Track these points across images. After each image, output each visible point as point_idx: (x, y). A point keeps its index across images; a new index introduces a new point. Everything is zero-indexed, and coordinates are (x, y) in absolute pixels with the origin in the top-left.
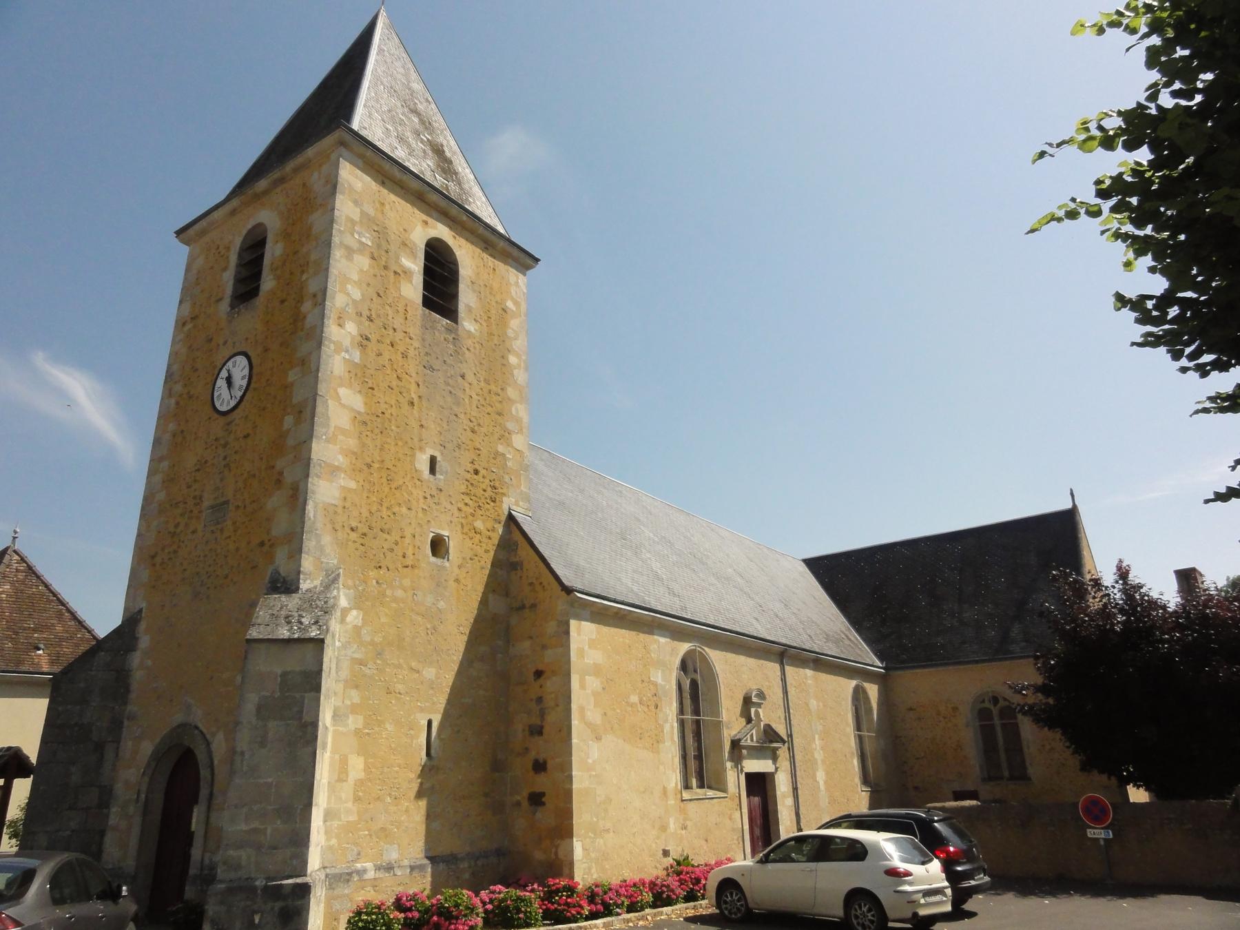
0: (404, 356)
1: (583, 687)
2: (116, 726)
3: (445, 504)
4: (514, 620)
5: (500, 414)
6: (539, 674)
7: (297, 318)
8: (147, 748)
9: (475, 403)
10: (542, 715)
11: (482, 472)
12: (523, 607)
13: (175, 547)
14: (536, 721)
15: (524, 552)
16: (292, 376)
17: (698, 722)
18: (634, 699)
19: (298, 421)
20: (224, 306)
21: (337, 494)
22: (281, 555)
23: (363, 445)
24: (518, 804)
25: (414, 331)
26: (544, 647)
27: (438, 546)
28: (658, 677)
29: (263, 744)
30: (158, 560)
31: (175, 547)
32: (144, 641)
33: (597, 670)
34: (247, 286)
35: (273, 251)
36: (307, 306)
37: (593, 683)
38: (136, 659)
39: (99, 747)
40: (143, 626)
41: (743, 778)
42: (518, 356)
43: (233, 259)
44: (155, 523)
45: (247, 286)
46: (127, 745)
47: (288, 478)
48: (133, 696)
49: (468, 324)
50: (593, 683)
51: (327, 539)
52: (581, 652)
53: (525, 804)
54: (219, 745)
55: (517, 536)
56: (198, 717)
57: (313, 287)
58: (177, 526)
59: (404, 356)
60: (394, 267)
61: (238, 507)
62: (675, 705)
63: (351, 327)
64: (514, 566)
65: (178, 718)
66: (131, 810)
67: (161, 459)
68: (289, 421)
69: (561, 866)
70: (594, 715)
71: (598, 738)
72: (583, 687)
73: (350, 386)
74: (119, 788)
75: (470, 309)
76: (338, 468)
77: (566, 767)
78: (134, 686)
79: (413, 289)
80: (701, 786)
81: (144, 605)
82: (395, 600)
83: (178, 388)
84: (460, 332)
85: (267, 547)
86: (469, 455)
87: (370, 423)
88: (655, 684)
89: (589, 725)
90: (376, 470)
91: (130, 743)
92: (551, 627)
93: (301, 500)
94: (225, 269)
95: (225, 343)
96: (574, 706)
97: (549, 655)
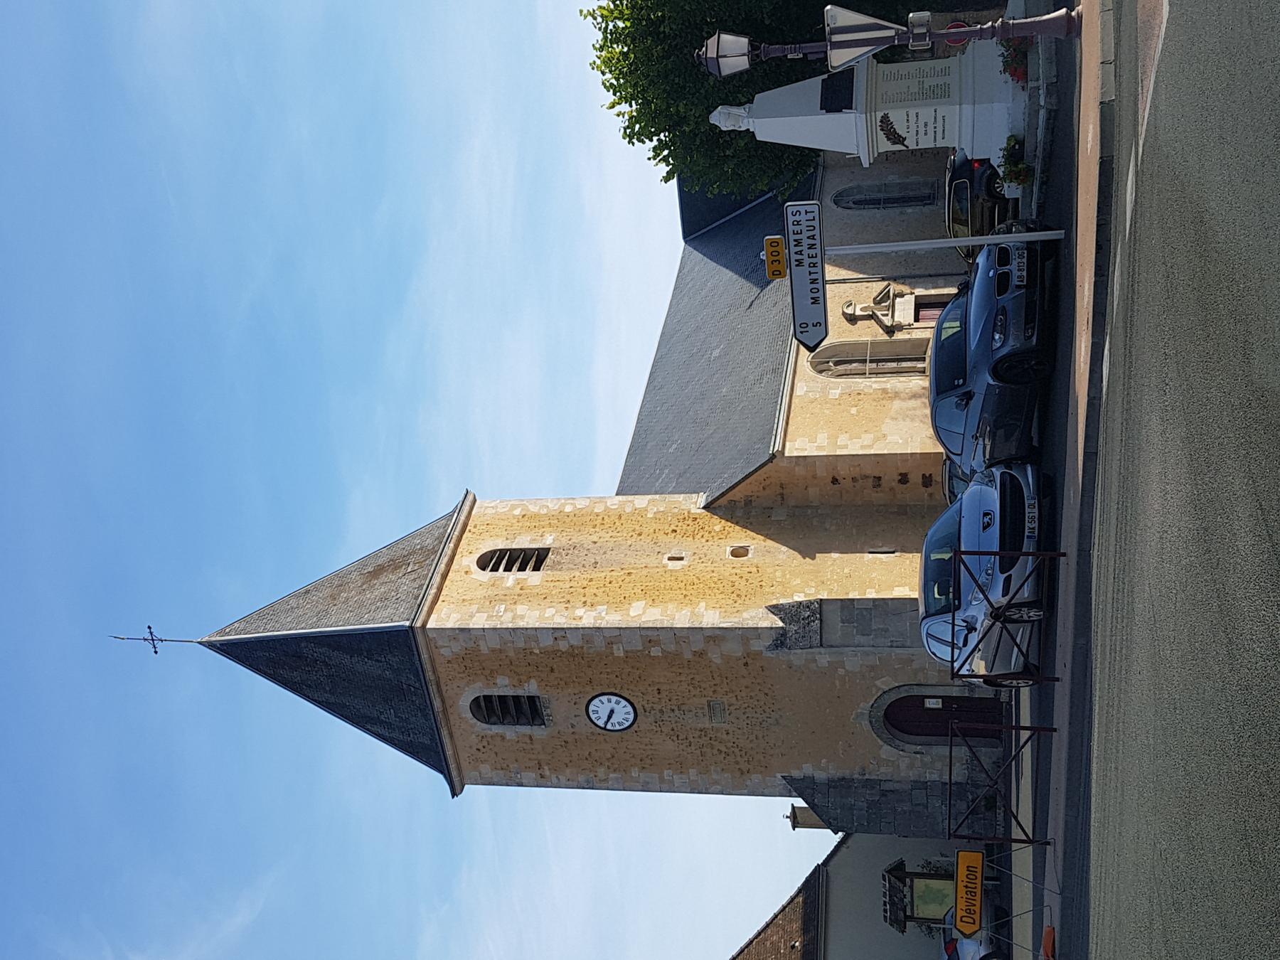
0: (591, 580)
1: (846, 447)
2: (869, 784)
3: (704, 550)
4: (792, 503)
5: (620, 517)
6: (835, 481)
7: (572, 654)
8: (886, 751)
9: (615, 534)
10: (867, 477)
11: (673, 527)
12: (782, 495)
13: (736, 750)
14: (870, 482)
15: (737, 494)
16: (619, 652)
17: (871, 361)
18: (854, 410)
19: (657, 643)
20: (538, 732)
21: (711, 612)
22: (757, 646)
23: (671, 600)
24: (931, 495)
25: (565, 575)
26: (814, 477)
27: (739, 552)
28: (835, 393)
29: (887, 630)
30: (744, 766)
31: (736, 750)
32: (808, 769)
33: (833, 438)
34: (523, 710)
35: (503, 687)
36: (563, 646)
37: (842, 439)
38: (820, 776)
39: (884, 793)
40: (796, 774)
41: (916, 325)
42: (564, 505)
43: (496, 729)
44: (715, 776)
45: (523, 710)
46: (884, 771)
47: (698, 647)
48: (847, 774)
49: (548, 541)
50: (842, 439)
51: (745, 615)
52: (819, 448)
53: (930, 490)
54: (884, 683)
55: (723, 501)
56: (865, 706)
57: (547, 642)
58: (720, 751)
59: (591, 580)
60: (518, 590)
61: (714, 692)
62: (859, 380)
63: (580, 612)
64: (748, 502)
65: (865, 723)
66: (927, 759)
67: (662, 780)
68: (656, 652)
69: (746, 71)
70: (867, 439)
71: (884, 436)
72: (846, 447)
73: (628, 610)
74: (912, 775)
75: (533, 540)
76: (692, 612)
77: (904, 457)
78: (839, 774)
79: (531, 578)
80: (924, 359)
81: (779, 776)
82: (784, 576)
83: (601, 772)
84: (557, 545)
85: (749, 659)
86: (661, 537)
87: (653, 595)
88: (841, 395)
89: (877, 439)
90: (689, 591)
91: (883, 770)
92: (800, 471)
93: (718, 632)
94: (503, 738)
95: (573, 726)
96: (860, 452)
97: (821, 472)
